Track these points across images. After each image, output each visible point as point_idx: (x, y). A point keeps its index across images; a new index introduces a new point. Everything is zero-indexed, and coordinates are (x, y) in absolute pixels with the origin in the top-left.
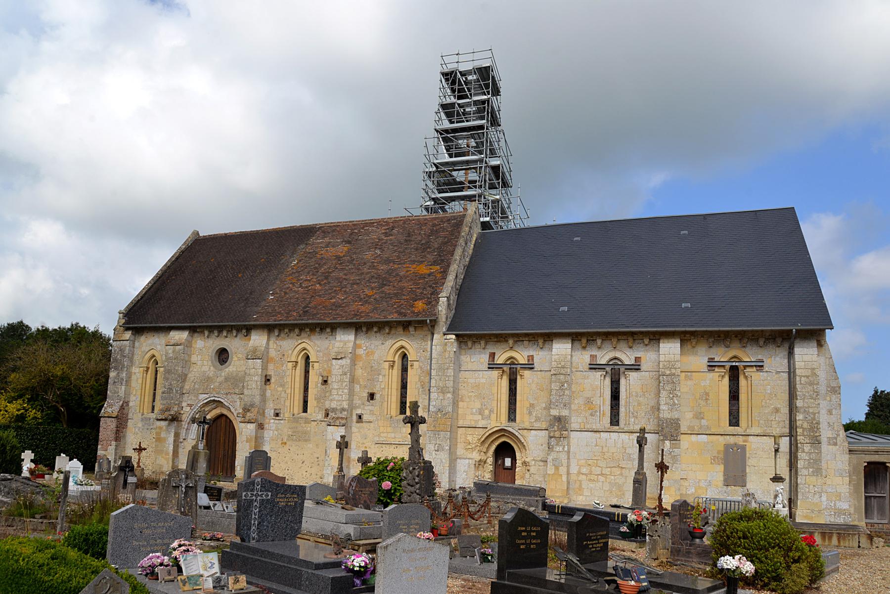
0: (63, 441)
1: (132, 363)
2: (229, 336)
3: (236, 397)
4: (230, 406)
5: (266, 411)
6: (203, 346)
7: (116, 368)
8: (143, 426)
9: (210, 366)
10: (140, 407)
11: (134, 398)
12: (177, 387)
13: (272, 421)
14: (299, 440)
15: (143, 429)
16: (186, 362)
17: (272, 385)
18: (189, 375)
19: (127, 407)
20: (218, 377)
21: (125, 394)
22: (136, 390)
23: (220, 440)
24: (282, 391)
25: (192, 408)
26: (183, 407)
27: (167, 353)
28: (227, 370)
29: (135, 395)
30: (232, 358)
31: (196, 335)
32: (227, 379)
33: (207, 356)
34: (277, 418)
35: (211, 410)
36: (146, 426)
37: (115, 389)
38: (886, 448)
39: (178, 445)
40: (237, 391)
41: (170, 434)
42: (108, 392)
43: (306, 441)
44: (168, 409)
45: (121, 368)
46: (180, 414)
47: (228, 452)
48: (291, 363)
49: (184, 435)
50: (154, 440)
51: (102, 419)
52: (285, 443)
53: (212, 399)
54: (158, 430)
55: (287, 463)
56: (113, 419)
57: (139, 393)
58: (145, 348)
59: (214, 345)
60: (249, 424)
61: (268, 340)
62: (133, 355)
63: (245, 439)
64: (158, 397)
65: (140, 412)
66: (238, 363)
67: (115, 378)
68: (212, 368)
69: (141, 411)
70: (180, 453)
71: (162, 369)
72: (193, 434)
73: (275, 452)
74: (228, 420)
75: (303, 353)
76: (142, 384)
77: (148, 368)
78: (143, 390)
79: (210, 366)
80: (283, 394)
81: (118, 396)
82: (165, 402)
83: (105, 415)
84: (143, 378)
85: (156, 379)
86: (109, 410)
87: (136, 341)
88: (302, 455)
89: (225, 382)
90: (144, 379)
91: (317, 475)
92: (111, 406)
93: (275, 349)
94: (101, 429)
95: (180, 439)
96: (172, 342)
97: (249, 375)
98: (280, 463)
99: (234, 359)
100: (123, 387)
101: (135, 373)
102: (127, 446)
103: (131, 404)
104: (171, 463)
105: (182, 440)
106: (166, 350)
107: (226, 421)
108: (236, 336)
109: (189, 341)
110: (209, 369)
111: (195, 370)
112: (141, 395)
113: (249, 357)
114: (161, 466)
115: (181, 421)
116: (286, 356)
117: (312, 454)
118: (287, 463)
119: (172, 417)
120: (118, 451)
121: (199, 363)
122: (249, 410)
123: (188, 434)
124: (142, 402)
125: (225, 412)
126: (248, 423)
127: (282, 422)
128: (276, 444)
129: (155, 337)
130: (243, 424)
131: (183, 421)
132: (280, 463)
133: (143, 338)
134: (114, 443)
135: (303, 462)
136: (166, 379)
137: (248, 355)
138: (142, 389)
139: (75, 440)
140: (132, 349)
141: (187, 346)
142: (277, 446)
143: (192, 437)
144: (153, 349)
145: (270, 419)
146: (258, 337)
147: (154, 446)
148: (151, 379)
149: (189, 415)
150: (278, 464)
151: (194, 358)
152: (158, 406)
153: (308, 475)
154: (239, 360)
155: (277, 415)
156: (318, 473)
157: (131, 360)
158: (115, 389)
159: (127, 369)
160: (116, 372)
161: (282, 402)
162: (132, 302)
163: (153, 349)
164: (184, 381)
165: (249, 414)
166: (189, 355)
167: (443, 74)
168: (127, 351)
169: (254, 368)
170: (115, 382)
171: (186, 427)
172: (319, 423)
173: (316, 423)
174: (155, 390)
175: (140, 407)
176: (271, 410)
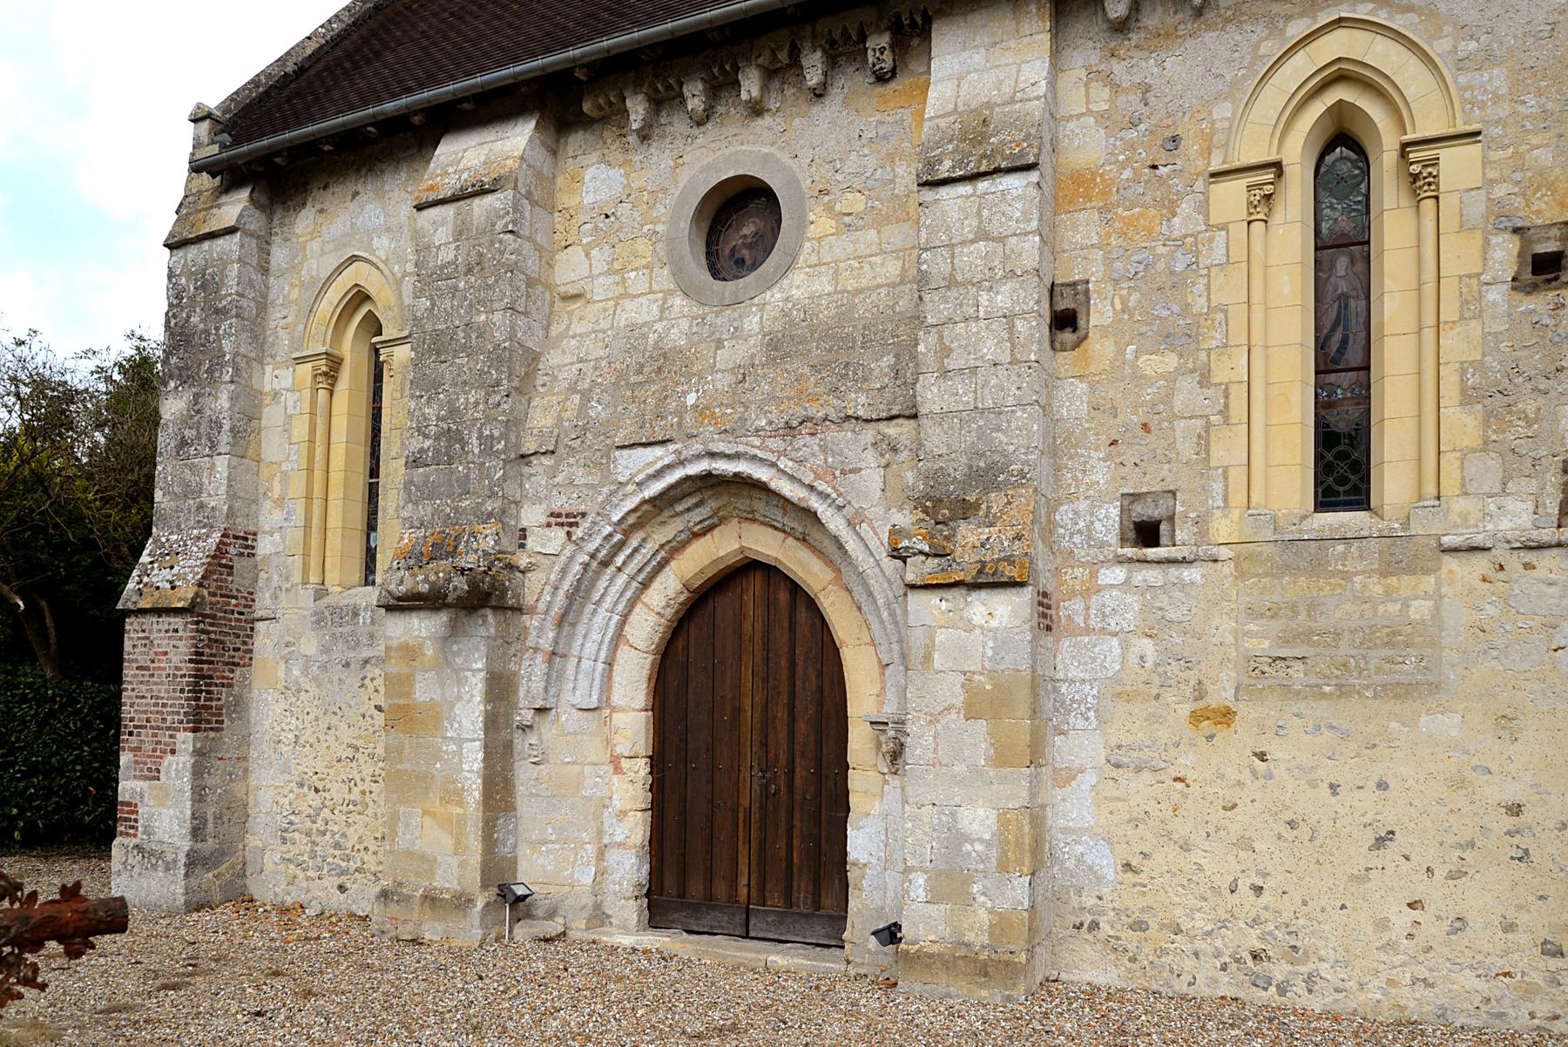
0: (39, 732)
1: (261, 347)
2: (773, 103)
3: (855, 445)
4: (815, 504)
5: (1064, 514)
6: (617, 190)
8: (325, 650)
9: (668, 293)
10: (306, 555)
11: (277, 516)
12: (489, 419)
13: (1118, 574)
14: (1343, 691)
15: (324, 667)
16: (531, 283)
17: (1100, 347)
18: (552, 359)
19: (245, 562)
20: (719, 344)
21: (232, 496)
22: (285, 479)
23: (738, 711)
24: (1180, 372)
25: (578, 533)
26: (523, 533)
27: (423, 250)
28: (775, 296)
29: (280, 502)
30: (802, 224)
31: (576, 140)
32: (777, 347)
33: (642, 246)
34: (1151, 552)
35: (684, 544)
36: (340, 652)
37: (187, 475)
39: (509, 746)
40: (859, 403)
41: (461, 681)
43: (1403, 691)
44: (443, 548)
45: (210, 371)
46: (510, 567)
47: (791, 774)
48: (1240, 184)
49: (537, 685)
50: (380, 719)
51: (131, 624)
52: (1225, 716)
53: (693, 469)
54: (393, 667)
55: (1245, 844)
56: (178, 622)
57: (298, 487)
58: (318, 264)
59: (684, 177)
60: (975, 596)
61: (1056, 68)
62: (263, 305)
63: (959, 701)
64: (390, 500)
65: (305, 582)
66: (841, 247)
67: (185, 421)
68: (678, 301)
69: (314, 578)
70: (521, 790)
71: (402, 354)
72: (583, 683)
73: (1147, 776)
74: (783, 597)
75: (1318, 108)
76: (312, 441)
77: (335, 363)
78: (318, 475)
79: (668, 293)
80: (1187, 393)
81: (201, 506)
82: (425, 510)
83: (143, 604)
84: (312, 414)
85: (373, 493)
86: (160, 577)
87: (277, 239)
88: (1370, 796)
89: (772, 362)
90: (321, 422)
91: (1509, 927)
92: (168, 556)
93: (1101, 117)
94: (129, 673)
95: (514, 707)
96: (448, 186)
97: (952, 283)
98: (1186, 847)
99: (812, 231)
100: (221, 463)
101: (276, 395)
102: (254, 754)
103: (264, 546)
104: (475, 844)
105: (527, 716)
106: (417, 235)
107: (770, 604)
108: (819, 94)
109: (539, 175)
110: (662, 310)
111: (577, 328)
112: (309, 498)
113: (944, 170)
114: (428, 863)
115: (518, 610)
116: (1191, 147)
117: (1459, 783)
118: (1245, 844)
119: (474, 585)
120: (209, 781)
121: (601, 288)
122: (965, 510)
123: (561, 676)
124: (314, 529)
125: (766, 544)
126: (975, 586)
127: (1190, 574)
128: (1152, 719)
129: (362, 198)
130: (933, 599)
131: (532, 611)
132: (1186, 847)
133: (305, 221)
134: (185, 740)
135: (1380, 842)
136: (425, 385)
137: (931, 165)
138: (310, 470)
139: (88, 726)
140: (257, 277)
141: (529, 195)
142: (1163, 735)
143: (580, 699)
144: (354, 259)
145: (1094, 566)
146: (978, 58)
147: (380, 751)
148: (347, 485)
149: (564, 571)
150: (1172, 851)
151: (570, 269)
152: (393, 537)
153: (1433, 930)
154: (848, 224)
155: (1147, 533)
156: (1523, 918)
157: (256, 329)
158: (187, 475)
159: (237, 370)
161: (1187, 449)
162: (255, 82)
163: (354, 259)
164: (524, 387)
165: (968, 534)
166: (539, 249)
168: (231, 286)
169: (982, 235)
170: (183, 443)
171: (546, 643)
172: (1514, 562)
173: (1481, 563)
174: (374, 472)
175: (306, 555)
176: (1101, 499)
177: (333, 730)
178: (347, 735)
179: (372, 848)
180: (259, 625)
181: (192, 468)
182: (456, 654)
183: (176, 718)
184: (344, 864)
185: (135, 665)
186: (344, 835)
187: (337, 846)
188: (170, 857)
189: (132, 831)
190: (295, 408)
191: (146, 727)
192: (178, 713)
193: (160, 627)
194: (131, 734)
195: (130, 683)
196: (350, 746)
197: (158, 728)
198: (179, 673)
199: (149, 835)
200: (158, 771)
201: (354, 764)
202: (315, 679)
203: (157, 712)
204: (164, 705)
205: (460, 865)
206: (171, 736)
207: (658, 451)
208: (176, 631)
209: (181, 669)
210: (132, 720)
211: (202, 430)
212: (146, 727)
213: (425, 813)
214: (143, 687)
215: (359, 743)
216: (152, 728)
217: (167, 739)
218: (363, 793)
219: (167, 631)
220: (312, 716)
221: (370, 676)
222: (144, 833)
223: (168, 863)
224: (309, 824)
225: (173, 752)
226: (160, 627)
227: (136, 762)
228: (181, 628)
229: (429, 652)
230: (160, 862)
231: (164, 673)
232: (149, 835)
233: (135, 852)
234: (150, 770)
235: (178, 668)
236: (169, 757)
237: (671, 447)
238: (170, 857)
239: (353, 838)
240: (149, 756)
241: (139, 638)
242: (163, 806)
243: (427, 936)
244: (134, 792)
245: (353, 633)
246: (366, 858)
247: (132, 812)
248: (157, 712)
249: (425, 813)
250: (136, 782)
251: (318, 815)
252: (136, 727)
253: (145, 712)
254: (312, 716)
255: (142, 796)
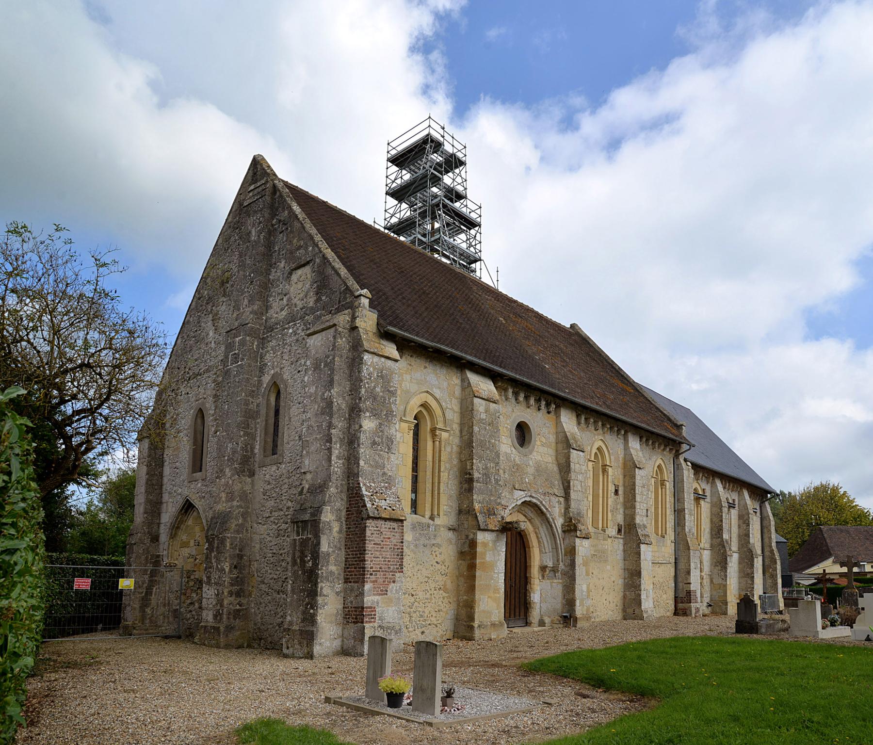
7: (375, 415)
15: (416, 546)
30: (535, 441)
36: (423, 540)
37: (377, 458)
38: (518, 557)
42: (362, 463)
51: (369, 523)
81: (384, 474)
94: (369, 546)
160: (377, 422)
167: (462, 163)
177: (420, 571)
178: (425, 573)
179: (434, 615)
180: (369, 523)
181: (379, 455)
182: (498, 546)
183: (395, 567)
184: (424, 623)
185: (373, 542)
186: (424, 612)
187: (421, 616)
188: (397, 628)
189: (372, 620)
190: (400, 439)
191: (379, 571)
192: (396, 565)
193: (386, 526)
194: (371, 574)
195: (369, 551)
196: (426, 577)
197: (386, 571)
198: (396, 547)
199: (382, 620)
200: (387, 591)
201: (427, 584)
202: (412, 550)
203: (386, 564)
204: (389, 561)
205: (499, 613)
206: (393, 575)
207: (523, 493)
208: (394, 529)
209: (397, 546)
210: (371, 568)
211: (384, 440)
212: (379, 571)
213: (489, 597)
214: (378, 553)
215: (430, 576)
216: (383, 571)
217: (391, 576)
218: (431, 594)
219: (390, 528)
220: (411, 566)
221: (434, 550)
222: (379, 620)
223: (397, 631)
224: (409, 610)
225: (394, 582)
226: (386, 526)
227: (374, 588)
228: (396, 528)
229: (491, 545)
230: (393, 631)
231: (389, 547)
232: (382, 620)
233: (379, 629)
234: (382, 591)
235: (395, 545)
236: (392, 584)
237: (526, 492)
238: (397, 628)
239: (427, 612)
240: (381, 584)
241: (375, 530)
242: (389, 606)
243: (493, 637)
244: (373, 602)
245: (427, 534)
246: (432, 619)
247: (372, 611)
248: (386, 564)
249: (489, 597)
250: (374, 597)
251: (413, 605)
252: (373, 571)
253: (379, 564)
254: (411, 566)
255: (378, 603)
